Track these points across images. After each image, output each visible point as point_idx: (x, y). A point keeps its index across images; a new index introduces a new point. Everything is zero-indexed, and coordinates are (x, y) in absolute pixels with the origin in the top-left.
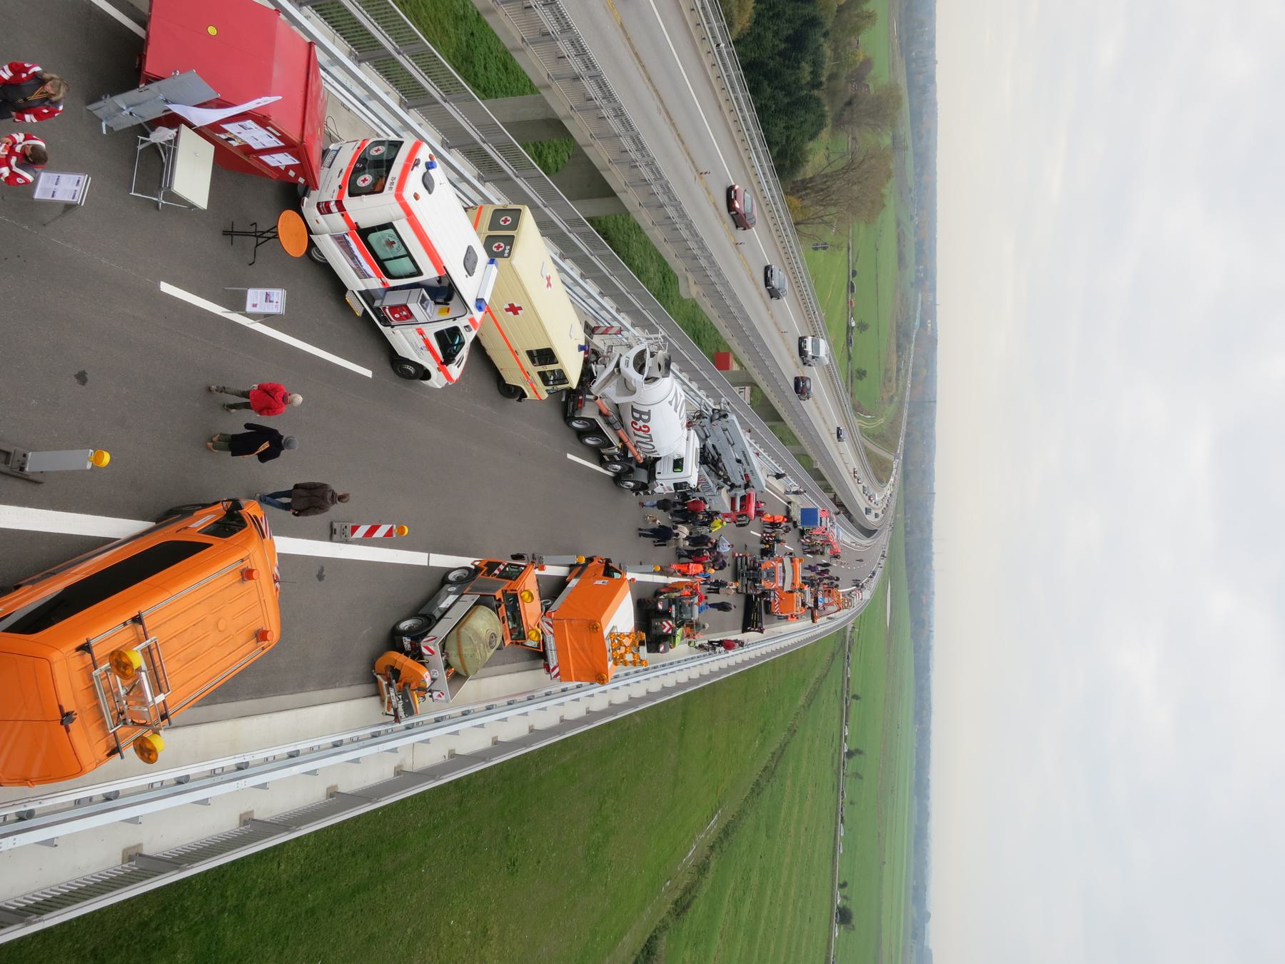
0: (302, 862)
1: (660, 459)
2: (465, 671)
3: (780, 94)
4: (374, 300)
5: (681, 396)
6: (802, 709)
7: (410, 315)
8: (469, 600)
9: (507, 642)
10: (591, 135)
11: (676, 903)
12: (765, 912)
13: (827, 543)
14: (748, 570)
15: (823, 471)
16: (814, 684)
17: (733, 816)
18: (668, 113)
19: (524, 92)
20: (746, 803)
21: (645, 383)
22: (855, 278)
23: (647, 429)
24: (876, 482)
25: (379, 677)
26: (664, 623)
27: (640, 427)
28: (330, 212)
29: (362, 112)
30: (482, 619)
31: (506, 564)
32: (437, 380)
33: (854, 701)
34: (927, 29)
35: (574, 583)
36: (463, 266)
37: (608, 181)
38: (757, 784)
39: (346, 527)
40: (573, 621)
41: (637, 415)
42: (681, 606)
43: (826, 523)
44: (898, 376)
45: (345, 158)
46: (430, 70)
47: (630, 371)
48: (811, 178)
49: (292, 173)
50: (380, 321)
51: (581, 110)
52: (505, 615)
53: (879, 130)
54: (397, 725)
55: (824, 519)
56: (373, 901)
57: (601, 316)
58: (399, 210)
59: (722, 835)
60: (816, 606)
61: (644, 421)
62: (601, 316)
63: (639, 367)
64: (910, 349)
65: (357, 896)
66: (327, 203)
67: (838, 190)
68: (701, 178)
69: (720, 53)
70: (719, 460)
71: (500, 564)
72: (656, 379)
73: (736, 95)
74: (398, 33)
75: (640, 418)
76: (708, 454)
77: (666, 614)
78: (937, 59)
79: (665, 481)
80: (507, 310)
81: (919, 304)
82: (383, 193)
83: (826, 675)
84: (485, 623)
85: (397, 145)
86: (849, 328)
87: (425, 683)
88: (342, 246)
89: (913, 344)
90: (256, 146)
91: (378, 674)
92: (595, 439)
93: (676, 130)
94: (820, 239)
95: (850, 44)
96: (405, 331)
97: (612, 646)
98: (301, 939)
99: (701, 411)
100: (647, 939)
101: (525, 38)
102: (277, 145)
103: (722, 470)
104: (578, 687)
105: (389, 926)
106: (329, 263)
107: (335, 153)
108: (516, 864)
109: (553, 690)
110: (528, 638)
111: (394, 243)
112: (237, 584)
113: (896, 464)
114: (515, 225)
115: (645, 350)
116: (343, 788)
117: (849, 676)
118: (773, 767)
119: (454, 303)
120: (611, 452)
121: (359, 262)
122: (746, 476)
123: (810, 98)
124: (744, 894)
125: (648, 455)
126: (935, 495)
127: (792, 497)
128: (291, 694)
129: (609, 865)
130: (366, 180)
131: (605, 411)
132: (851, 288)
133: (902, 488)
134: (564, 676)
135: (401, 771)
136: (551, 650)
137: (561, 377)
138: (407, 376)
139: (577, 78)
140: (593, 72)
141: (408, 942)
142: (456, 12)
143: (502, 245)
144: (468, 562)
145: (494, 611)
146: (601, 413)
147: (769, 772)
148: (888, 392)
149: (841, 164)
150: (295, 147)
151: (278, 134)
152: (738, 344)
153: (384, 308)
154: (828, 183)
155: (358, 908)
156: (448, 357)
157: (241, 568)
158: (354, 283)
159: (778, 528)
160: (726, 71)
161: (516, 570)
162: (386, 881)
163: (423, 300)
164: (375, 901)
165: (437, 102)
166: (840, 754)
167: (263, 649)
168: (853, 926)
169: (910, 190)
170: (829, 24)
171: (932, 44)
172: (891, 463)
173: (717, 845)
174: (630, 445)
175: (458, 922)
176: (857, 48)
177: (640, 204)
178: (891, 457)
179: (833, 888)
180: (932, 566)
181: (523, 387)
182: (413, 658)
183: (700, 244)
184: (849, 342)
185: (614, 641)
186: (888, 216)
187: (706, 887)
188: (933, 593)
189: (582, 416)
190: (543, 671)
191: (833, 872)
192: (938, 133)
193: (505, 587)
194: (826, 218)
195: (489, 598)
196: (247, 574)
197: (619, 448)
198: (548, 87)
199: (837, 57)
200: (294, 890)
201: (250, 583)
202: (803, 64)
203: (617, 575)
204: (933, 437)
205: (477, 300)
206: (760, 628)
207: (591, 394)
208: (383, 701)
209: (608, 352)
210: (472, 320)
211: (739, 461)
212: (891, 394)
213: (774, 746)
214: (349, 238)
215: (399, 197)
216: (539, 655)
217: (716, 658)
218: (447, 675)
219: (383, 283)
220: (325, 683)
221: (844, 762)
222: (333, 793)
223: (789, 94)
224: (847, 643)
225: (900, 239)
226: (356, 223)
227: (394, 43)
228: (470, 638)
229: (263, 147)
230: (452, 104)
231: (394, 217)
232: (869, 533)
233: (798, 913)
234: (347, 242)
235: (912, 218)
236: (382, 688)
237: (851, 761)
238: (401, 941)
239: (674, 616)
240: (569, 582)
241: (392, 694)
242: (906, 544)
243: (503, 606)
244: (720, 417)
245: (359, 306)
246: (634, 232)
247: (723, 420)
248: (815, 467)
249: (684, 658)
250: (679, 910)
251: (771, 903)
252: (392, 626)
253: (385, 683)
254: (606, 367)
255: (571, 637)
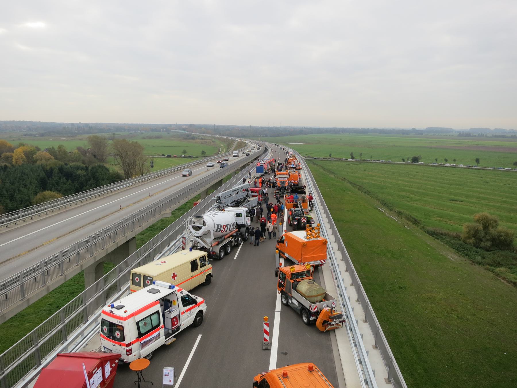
0: (405, 375)
1: (236, 223)
2: (324, 294)
3: (89, 182)
4: (169, 333)
5: (211, 212)
6: (336, 176)
7: (175, 317)
8: (294, 293)
9: (311, 278)
10: (103, 249)
11: (413, 224)
12: (415, 190)
13: (270, 163)
14: (281, 192)
15: (242, 165)
16: (326, 171)
17: (378, 202)
18: (95, 221)
19: (83, 286)
20: (373, 197)
21: (206, 226)
22: (165, 154)
23: (224, 226)
24: (246, 147)
25: (327, 329)
26: (302, 221)
27: (223, 229)
28: (131, 350)
29: (88, 338)
30: (302, 287)
31: (279, 279)
32: (203, 307)
33: (332, 156)
34: (66, 126)
35: (287, 255)
36: (155, 294)
37: (122, 244)
38: (365, 193)
39: (265, 344)
40: (302, 254)
41: (219, 230)
42: (296, 215)
43: (262, 164)
44: (204, 139)
45: (108, 344)
46: (72, 325)
47: (201, 232)
48: (124, 171)
49: (114, 365)
50: (178, 331)
51: (92, 253)
52: (300, 279)
53: (106, 144)
54: (346, 321)
55: (261, 164)
56: (420, 345)
57: (178, 246)
58: (132, 319)
59: (386, 206)
60: (295, 168)
61: (221, 227)
62: (178, 246)
63: (199, 229)
64: (194, 135)
65: (418, 351)
66: (127, 351)
67: (129, 160)
68: (123, 209)
69: (71, 201)
70: (237, 201)
71: (279, 282)
72: (204, 222)
73: (89, 195)
74: (55, 338)
75: (220, 229)
76: (235, 205)
77: (299, 221)
78: (79, 123)
79: (245, 220)
80: (174, 279)
81: (176, 131)
82: (123, 326)
83: (322, 167)
84: (304, 286)
85: (104, 322)
86: (185, 157)
87: (329, 309)
88: (146, 345)
89: (192, 133)
90: (101, 380)
91: (326, 329)
92: (228, 248)
93: (102, 218)
94: (149, 167)
95: (71, 156)
96: (182, 320)
97: (312, 238)
98: (437, 375)
99: (217, 207)
100: (428, 235)
101: (61, 274)
102: (101, 370)
103: (241, 200)
104: (329, 253)
105: (430, 338)
106: (153, 352)
107: (105, 349)
108: (401, 287)
109: (330, 262)
110: (309, 269)
111: (145, 322)
112: (289, 380)
113: (239, 140)
114: (139, 275)
115: (192, 226)
116: (373, 343)
117: (322, 158)
118: (359, 187)
119: (171, 298)
120: (233, 241)
121: (152, 338)
122: (243, 190)
123: (92, 171)
124: (408, 197)
125: (235, 227)
126: (251, 125)
127: (252, 177)
128: (335, 364)
129: (400, 250)
130: (118, 334)
131: (217, 243)
132: (169, 156)
133: (249, 138)
134: (324, 258)
135: (365, 320)
136: (314, 263)
137: (202, 258)
138: (201, 320)
139: (78, 254)
140: (77, 248)
141: (436, 330)
142: (47, 314)
143: (147, 281)
144: (279, 296)
145: (299, 283)
146: (217, 245)
147: (360, 188)
148: (210, 143)
149: (119, 160)
150: (102, 361)
151: (96, 369)
152: (190, 195)
153: (173, 328)
154: (127, 164)
155: (423, 351)
156: (194, 302)
157: (283, 378)
158: (161, 341)
159: (264, 181)
160: (79, 199)
161: (282, 275)
162: (411, 339)
163: (170, 311)
164: (420, 344)
165: (86, 308)
166: (353, 162)
167: (316, 369)
168: (419, 156)
169: (131, 134)
170: (62, 163)
171: (73, 124)
172: (238, 142)
173: (390, 208)
174: (231, 234)
175: (426, 310)
176: (72, 153)
177: (132, 231)
178: (236, 142)
179: (405, 164)
180: (279, 127)
181: (206, 276)
182: (319, 315)
183: (150, 208)
184: (190, 157)
185: (310, 237)
186: (141, 142)
187: (407, 212)
188: (289, 127)
189: (219, 252)
190: (323, 267)
191: (398, 164)
192: (108, 123)
193: (289, 279)
194: (141, 165)
195: (293, 285)
196: (285, 375)
197: (232, 239)
198: (82, 266)
199: (75, 160)
200: (417, 378)
201: (289, 374)
202: (78, 173)
203: (284, 238)
204: (228, 126)
205: (170, 289)
206: (304, 187)
207: (210, 249)
208: (337, 328)
209: (193, 242)
210: (179, 291)
211: (237, 193)
212: (211, 142)
213: (351, 186)
214: (142, 342)
215: (125, 319)
216: (316, 268)
217: (316, 203)
218: (324, 301)
219: (162, 328)
220: (330, 351)
221: (356, 160)
222: (376, 347)
223: (90, 179)
224: (309, 159)
225: (150, 138)
226: (136, 338)
227: (59, 324)
228: (310, 292)
229: (102, 376)
230: (87, 301)
231: (134, 321)
232: (266, 150)
233: (415, 177)
234: (144, 342)
235: (142, 133)
236: (332, 328)
237: (355, 157)
238: (435, 333)
239: (299, 218)
240: (287, 257)
241: (334, 323)
242: (271, 137)
243: (296, 280)
244: (220, 200)
245: (171, 339)
246: (144, 241)
247: (221, 198)
248: (240, 169)
249: (317, 215)
250: (416, 222)
251: (412, 187)
252: (306, 325)
253: (329, 327)
254: (199, 242)
255: (309, 254)
